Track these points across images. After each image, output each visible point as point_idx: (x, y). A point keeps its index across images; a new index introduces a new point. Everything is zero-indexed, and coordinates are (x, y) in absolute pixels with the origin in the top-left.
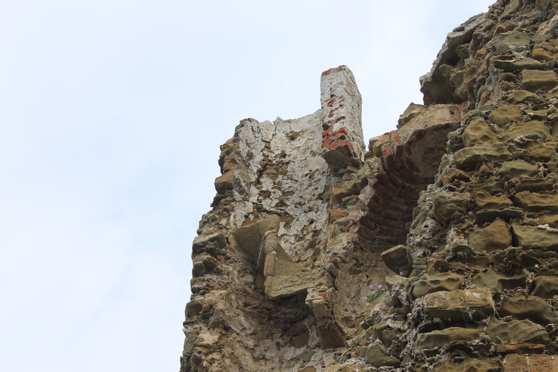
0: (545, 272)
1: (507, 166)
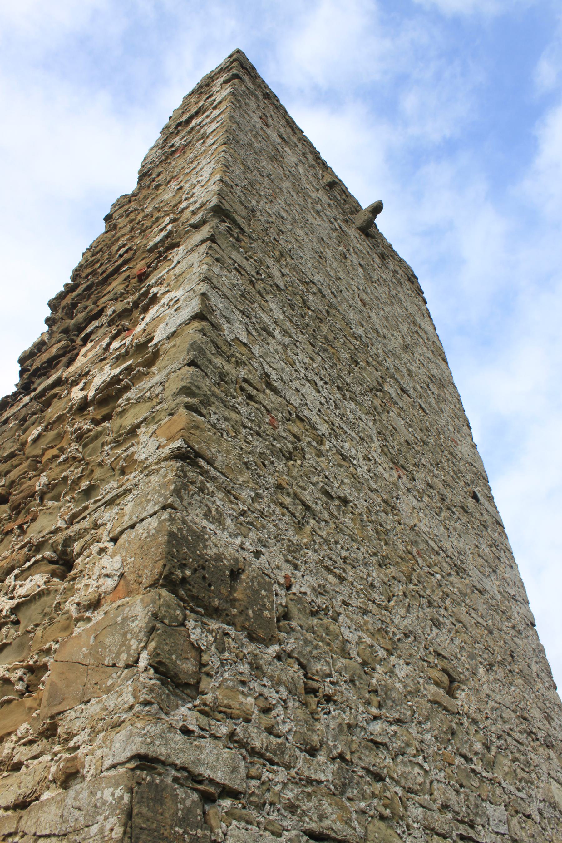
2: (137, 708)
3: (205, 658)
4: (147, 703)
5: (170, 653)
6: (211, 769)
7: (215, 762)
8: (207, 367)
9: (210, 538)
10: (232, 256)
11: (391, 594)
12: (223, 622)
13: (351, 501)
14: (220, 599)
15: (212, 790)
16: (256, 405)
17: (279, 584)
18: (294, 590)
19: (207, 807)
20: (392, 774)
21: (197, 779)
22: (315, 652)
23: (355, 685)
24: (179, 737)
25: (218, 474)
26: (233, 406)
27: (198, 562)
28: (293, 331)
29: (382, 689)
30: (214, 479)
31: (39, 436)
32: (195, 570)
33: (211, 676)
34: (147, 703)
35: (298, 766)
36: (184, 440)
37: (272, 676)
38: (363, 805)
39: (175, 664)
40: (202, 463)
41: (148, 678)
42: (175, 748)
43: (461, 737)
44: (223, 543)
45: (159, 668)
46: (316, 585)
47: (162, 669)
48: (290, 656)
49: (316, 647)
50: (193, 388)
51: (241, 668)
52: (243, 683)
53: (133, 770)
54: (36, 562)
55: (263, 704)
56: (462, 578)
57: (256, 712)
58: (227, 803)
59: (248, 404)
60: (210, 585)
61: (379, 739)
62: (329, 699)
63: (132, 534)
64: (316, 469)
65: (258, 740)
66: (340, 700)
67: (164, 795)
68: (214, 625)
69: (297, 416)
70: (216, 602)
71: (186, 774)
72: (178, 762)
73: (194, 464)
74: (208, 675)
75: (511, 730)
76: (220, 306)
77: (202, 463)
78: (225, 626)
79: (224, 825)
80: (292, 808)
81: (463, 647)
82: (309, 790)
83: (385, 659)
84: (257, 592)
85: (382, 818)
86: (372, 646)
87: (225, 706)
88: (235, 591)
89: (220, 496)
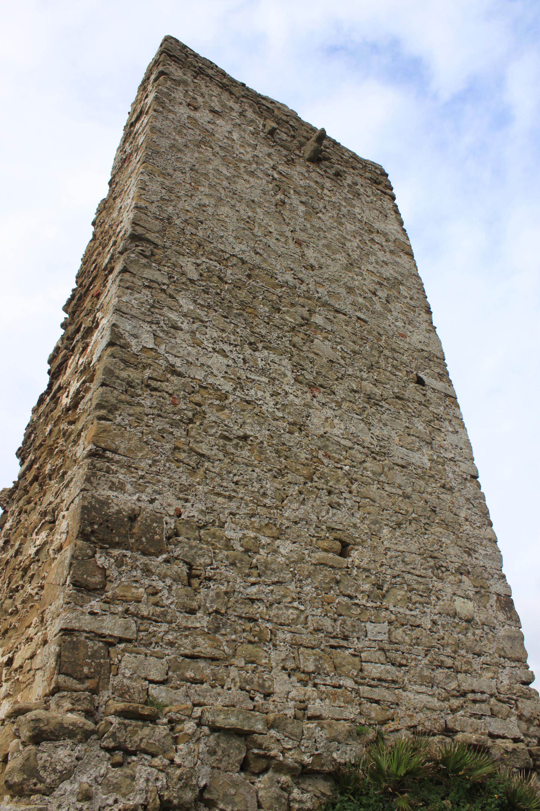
2: (64, 606)
3: (108, 572)
4: (68, 603)
5: (82, 575)
6: (110, 630)
7: (112, 625)
8: (114, 383)
9: (113, 501)
10: (144, 276)
11: (284, 496)
12: (123, 549)
13: (251, 436)
14: (119, 537)
15: (111, 640)
16: (158, 394)
17: (170, 516)
18: (183, 517)
19: (110, 649)
20: (264, 616)
21: (102, 636)
22: (200, 552)
23: (236, 566)
24: (88, 617)
25: (121, 457)
26: (138, 403)
27: (103, 518)
28: (203, 314)
29: (261, 565)
30: (117, 462)
31: (51, 431)
32: (101, 524)
33: (112, 582)
34: (68, 603)
35: (178, 621)
36: (94, 444)
37: (159, 574)
38: (233, 637)
39: (86, 580)
40: (108, 454)
41: (70, 590)
42: (87, 623)
43: (346, 583)
44: (123, 502)
45: (76, 584)
46: (204, 508)
47: (78, 584)
48: (177, 558)
49: (201, 549)
50: (103, 403)
51: (134, 573)
52: (136, 581)
53: (61, 636)
54: (43, 524)
55: (150, 591)
56: (380, 461)
57: (145, 596)
58: (122, 646)
59: (152, 396)
60: (112, 530)
61: (254, 597)
62: (209, 579)
63: (73, 505)
64: (216, 422)
65: (145, 610)
66: (219, 578)
67: (79, 645)
68: (116, 552)
69: (201, 387)
70: (117, 539)
71: (93, 634)
72: (87, 629)
73: (102, 456)
74: (111, 581)
75: (414, 569)
76: (128, 328)
77: (108, 454)
78: (124, 551)
79: (119, 656)
80: (171, 644)
81: (366, 517)
82: (187, 633)
83: (268, 544)
84: (150, 525)
85: (250, 642)
86: (256, 538)
87: (122, 596)
88: (134, 528)
89: (122, 472)
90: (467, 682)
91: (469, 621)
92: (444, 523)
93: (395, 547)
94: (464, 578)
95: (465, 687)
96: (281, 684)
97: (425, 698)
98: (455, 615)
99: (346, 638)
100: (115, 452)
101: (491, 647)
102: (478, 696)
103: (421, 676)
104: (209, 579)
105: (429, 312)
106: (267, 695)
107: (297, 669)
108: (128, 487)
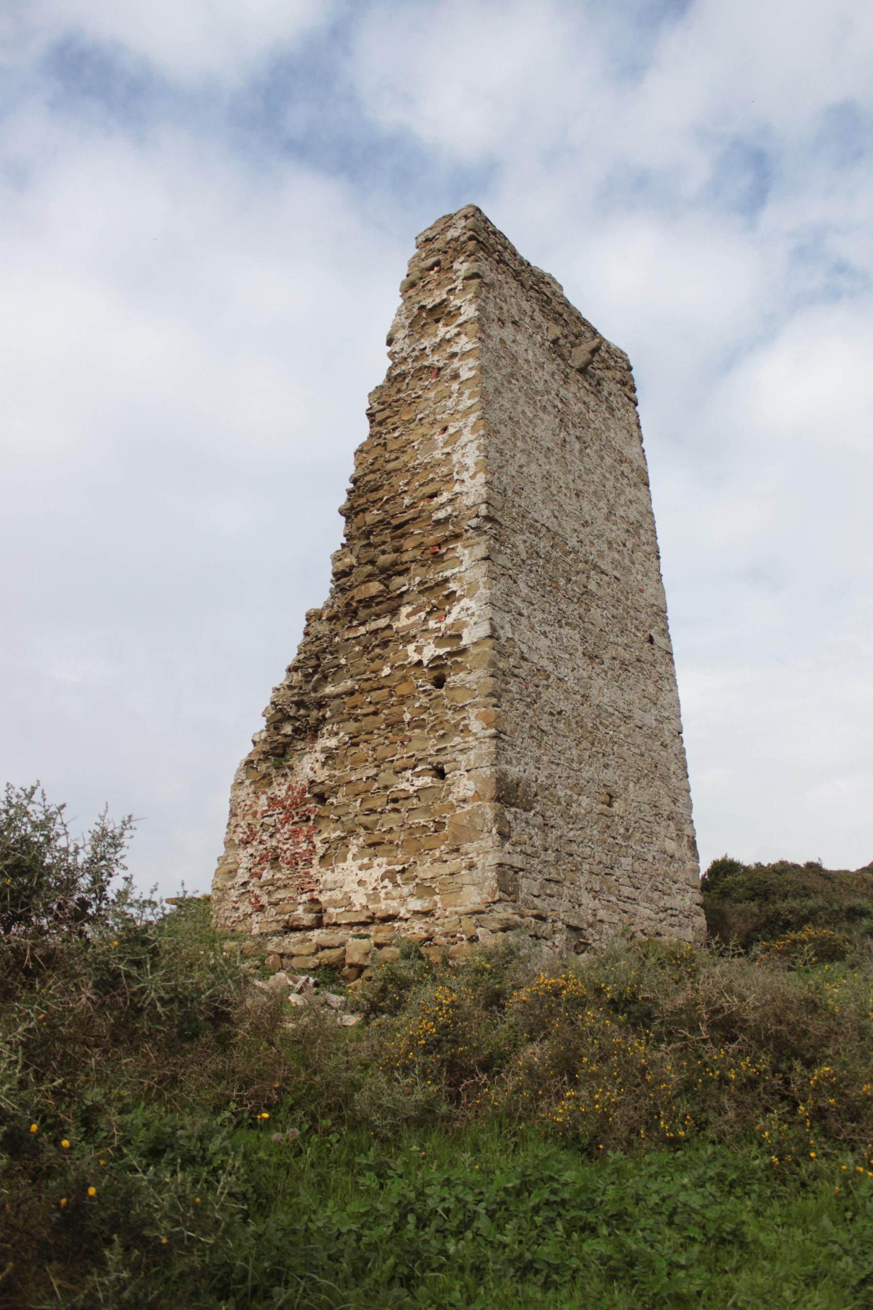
0: (378, 535)
1: (367, 478)
62: (552, 827)
68: (513, 809)
80: (540, 872)
90: (667, 901)
91: (671, 857)
92: (662, 778)
93: (635, 797)
94: (671, 823)
95: (668, 905)
96: (586, 899)
97: (648, 911)
98: (665, 852)
99: (612, 868)
100: (505, 734)
101: (682, 877)
102: (674, 912)
103: (647, 897)
104: (552, 827)
105: (658, 558)
106: (580, 905)
107: (591, 889)
108: (514, 761)
